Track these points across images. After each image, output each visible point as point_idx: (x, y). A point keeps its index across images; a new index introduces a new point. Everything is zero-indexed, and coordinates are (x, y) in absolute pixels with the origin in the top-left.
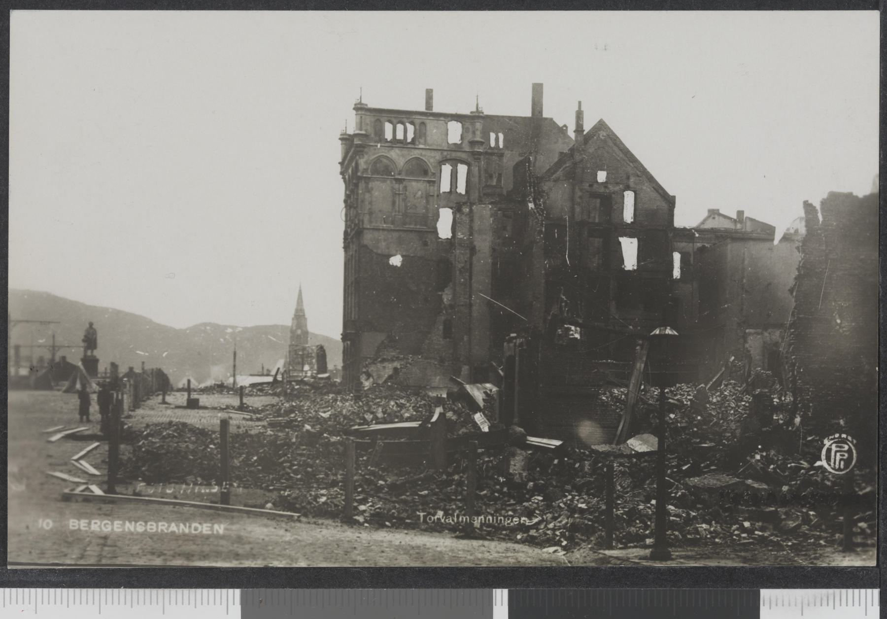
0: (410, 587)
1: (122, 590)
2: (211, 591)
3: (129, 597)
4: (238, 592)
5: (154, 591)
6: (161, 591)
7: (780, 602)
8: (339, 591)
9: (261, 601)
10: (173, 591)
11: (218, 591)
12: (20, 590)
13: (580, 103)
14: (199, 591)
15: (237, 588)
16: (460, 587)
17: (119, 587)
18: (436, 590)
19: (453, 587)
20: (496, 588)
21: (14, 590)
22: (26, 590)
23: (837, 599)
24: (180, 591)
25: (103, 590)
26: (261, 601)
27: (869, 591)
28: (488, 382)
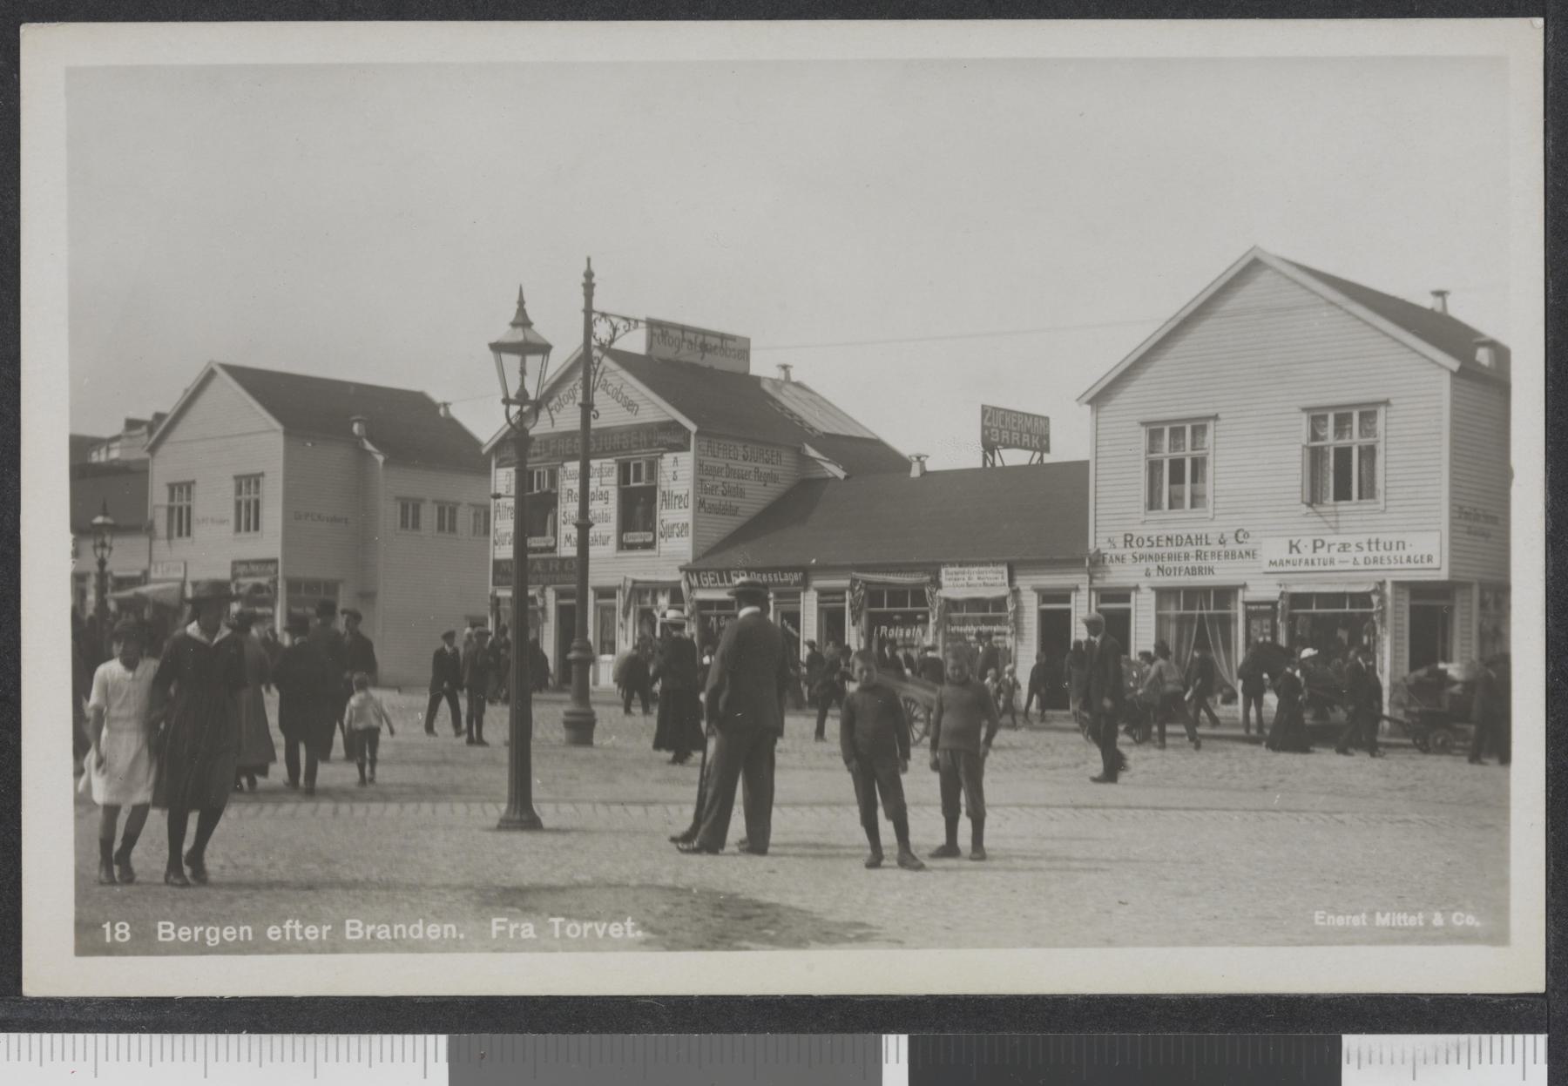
0: (739, 1030)
1: (244, 1037)
2: (398, 1038)
3: (299, 1048)
4: (443, 1039)
5: (299, 1038)
6: (310, 1038)
7: (1376, 1057)
8: (618, 1037)
9: (483, 1056)
10: (332, 1038)
11: (409, 1038)
12: (68, 1037)
13: (589, 260)
14: (376, 1038)
15: (442, 1033)
16: (826, 1032)
17: (239, 1031)
18: (784, 1036)
19: (812, 1031)
20: (887, 1032)
21: (57, 1036)
22: (79, 1036)
23: (1475, 1051)
24: (343, 1038)
25: (211, 1037)
26: (483, 1056)
27: (1530, 1037)
28: (348, 699)
